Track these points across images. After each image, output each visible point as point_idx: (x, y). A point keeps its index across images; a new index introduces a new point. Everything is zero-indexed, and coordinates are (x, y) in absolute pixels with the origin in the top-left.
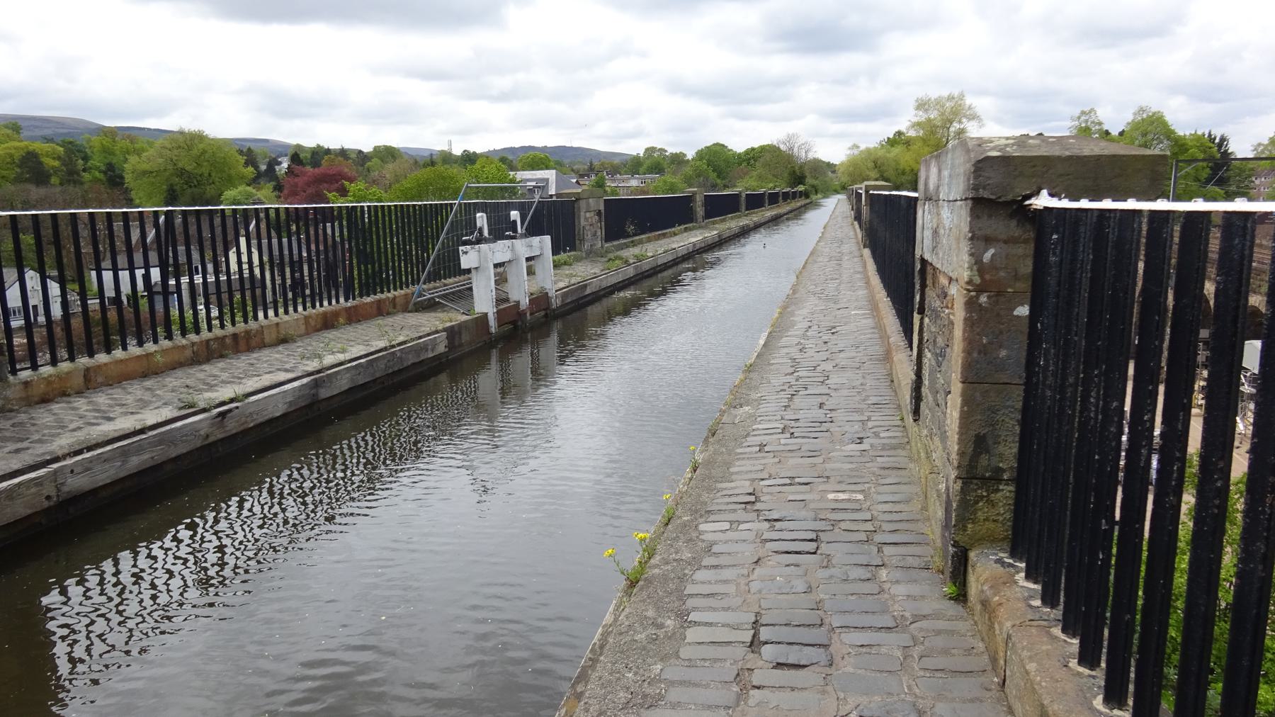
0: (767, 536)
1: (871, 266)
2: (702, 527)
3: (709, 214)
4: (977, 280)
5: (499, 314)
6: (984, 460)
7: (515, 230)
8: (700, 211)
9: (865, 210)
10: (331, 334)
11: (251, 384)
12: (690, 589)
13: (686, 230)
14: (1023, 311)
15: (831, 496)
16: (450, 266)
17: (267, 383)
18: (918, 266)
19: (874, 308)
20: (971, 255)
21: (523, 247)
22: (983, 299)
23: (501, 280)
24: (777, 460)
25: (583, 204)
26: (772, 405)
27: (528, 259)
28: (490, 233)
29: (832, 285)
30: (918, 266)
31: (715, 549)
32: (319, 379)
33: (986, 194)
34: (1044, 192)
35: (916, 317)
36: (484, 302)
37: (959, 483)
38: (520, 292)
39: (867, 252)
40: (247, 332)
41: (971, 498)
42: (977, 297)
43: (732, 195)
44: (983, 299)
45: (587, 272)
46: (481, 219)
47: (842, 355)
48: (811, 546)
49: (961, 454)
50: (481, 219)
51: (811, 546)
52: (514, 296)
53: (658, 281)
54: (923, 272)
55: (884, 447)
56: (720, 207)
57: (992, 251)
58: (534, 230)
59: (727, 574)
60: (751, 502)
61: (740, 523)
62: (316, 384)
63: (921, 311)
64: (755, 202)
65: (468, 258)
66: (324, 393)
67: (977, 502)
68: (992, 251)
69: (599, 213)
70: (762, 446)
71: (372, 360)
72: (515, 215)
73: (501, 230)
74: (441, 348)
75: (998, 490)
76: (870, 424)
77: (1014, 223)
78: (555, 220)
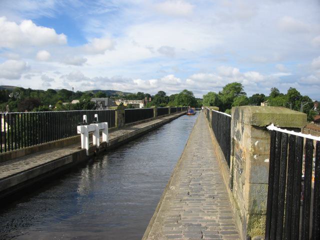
4: (253, 151)
5: (90, 149)
6: (256, 209)
9: (211, 115)
14: (267, 161)
20: (252, 143)
34: (272, 125)
35: (231, 157)
36: (85, 145)
37: (248, 215)
40: (6, 154)
41: (252, 220)
42: (253, 156)
45: (119, 133)
46: (85, 117)
50: (85, 117)
53: (141, 136)
56: (162, 112)
57: (257, 142)
58: (101, 120)
63: (233, 155)
64: (174, 111)
68: (257, 142)
69: (123, 114)
72: (96, 116)
73: (91, 120)
74: (71, 161)
75: (260, 218)
77: (264, 133)
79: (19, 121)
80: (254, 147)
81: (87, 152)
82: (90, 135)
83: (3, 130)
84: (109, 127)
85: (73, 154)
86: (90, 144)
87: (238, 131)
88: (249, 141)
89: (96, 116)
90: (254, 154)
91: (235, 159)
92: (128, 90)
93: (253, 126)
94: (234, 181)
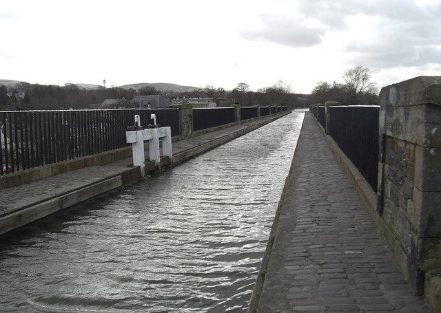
0: (319, 271)
1: (334, 144)
2: (286, 268)
3: (197, 127)
4: (429, 142)
7: (153, 123)
8: (238, 116)
10: (64, 175)
11: (30, 200)
12: (289, 297)
13: (232, 125)
15: (346, 252)
16: (122, 141)
17: (36, 201)
18: (381, 140)
19: (341, 163)
21: (156, 133)
22: (432, 151)
23: (147, 149)
24: (314, 236)
25: (183, 112)
26: (302, 211)
27: (160, 139)
28: (157, 123)
29: (315, 154)
30: (381, 140)
31: (296, 278)
32: (64, 198)
33: (432, 102)
35: (380, 165)
36: (138, 159)
38: (155, 156)
39: (329, 137)
43: (274, 103)
44: (432, 151)
46: (137, 118)
47: (331, 187)
48: (343, 275)
49: (422, 226)
50: (137, 118)
51: (343, 275)
52: (152, 158)
54: (384, 143)
55: (365, 229)
58: (161, 124)
59: (305, 289)
60: (307, 256)
61: (304, 266)
62: (61, 202)
63: (384, 161)
65: (131, 137)
66: (66, 205)
67: (429, 249)
69: (190, 116)
70: (304, 230)
71: (80, 192)
72: (153, 116)
73: (147, 123)
76: (355, 219)
78: (168, 118)
79: (49, 130)
80: (429, 136)
81: (142, 171)
82: (145, 143)
83: (3, 147)
84: (173, 135)
85: (124, 173)
86: (147, 159)
87: (397, 121)
88: (421, 129)
89: (153, 116)
90: (431, 147)
91: (387, 166)
92: (390, 58)
93: (429, 105)
94: (386, 201)
